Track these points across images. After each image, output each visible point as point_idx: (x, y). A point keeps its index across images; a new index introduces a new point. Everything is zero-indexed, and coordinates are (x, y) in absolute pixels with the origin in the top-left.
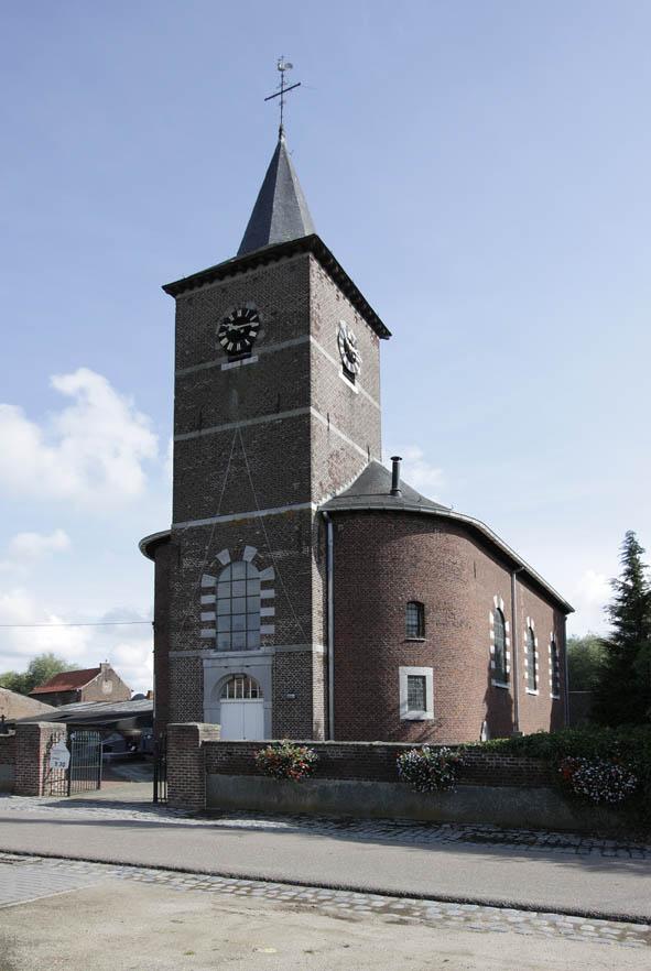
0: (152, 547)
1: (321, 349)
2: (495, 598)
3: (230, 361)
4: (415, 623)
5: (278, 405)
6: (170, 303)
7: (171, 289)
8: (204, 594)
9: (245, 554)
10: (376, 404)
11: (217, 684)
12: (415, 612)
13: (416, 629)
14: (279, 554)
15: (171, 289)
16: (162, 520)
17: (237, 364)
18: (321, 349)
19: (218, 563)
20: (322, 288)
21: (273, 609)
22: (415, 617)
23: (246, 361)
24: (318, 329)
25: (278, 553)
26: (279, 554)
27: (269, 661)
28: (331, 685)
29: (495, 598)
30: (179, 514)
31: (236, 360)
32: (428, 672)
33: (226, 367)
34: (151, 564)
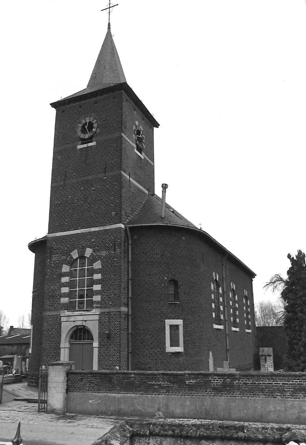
0: (35, 246)
1: (127, 138)
2: (214, 273)
3: (82, 144)
4: (173, 293)
5: (105, 169)
6: (54, 111)
7: (53, 105)
8: (63, 277)
9: (86, 253)
10: (152, 163)
11: (68, 333)
12: (173, 286)
13: (173, 296)
14: (104, 253)
15: (53, 105)
16: (41, 230)
17: (85, 146)
18: (127, 138)
19: (71, 257)
20: (127, 106)
21: (100, 275)
22: (173, 289)
23: (90, 144)
24: (125, 128)
25: (104, 252)
26: (104, 253)
27: (97, 318)
28: (130, 363)
29: (214, 273)
30: (52, 228)
31: (85, 143)
32: (180, 322)
33: (80, 147)
34: (33, 255)
